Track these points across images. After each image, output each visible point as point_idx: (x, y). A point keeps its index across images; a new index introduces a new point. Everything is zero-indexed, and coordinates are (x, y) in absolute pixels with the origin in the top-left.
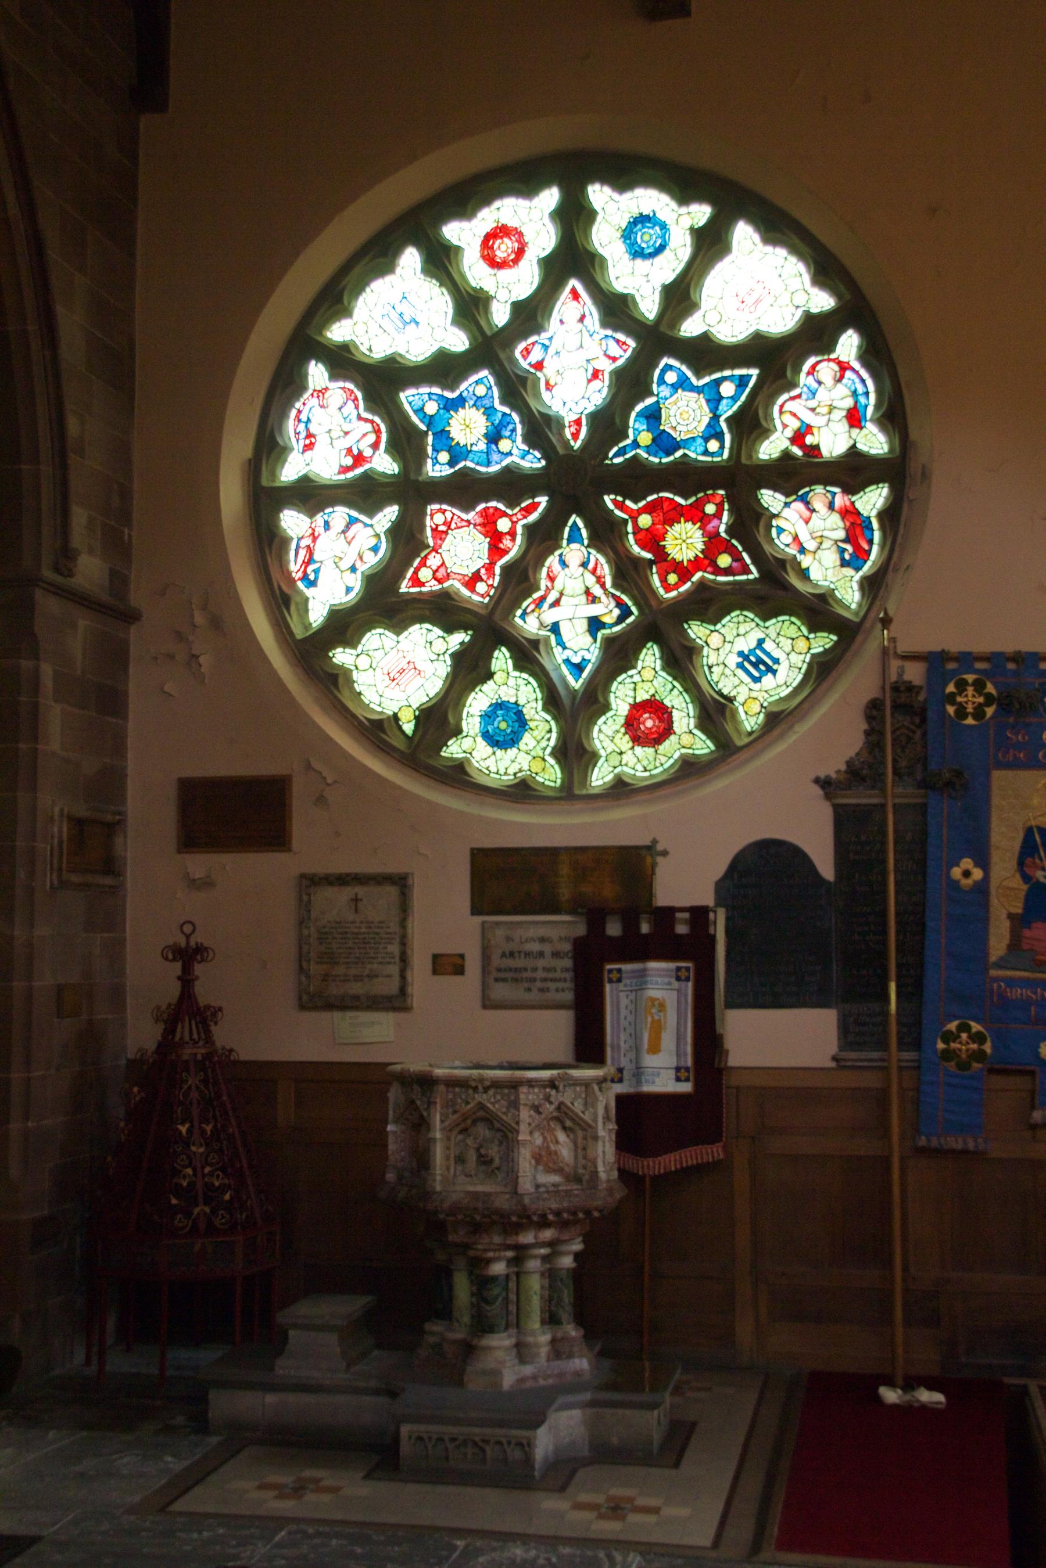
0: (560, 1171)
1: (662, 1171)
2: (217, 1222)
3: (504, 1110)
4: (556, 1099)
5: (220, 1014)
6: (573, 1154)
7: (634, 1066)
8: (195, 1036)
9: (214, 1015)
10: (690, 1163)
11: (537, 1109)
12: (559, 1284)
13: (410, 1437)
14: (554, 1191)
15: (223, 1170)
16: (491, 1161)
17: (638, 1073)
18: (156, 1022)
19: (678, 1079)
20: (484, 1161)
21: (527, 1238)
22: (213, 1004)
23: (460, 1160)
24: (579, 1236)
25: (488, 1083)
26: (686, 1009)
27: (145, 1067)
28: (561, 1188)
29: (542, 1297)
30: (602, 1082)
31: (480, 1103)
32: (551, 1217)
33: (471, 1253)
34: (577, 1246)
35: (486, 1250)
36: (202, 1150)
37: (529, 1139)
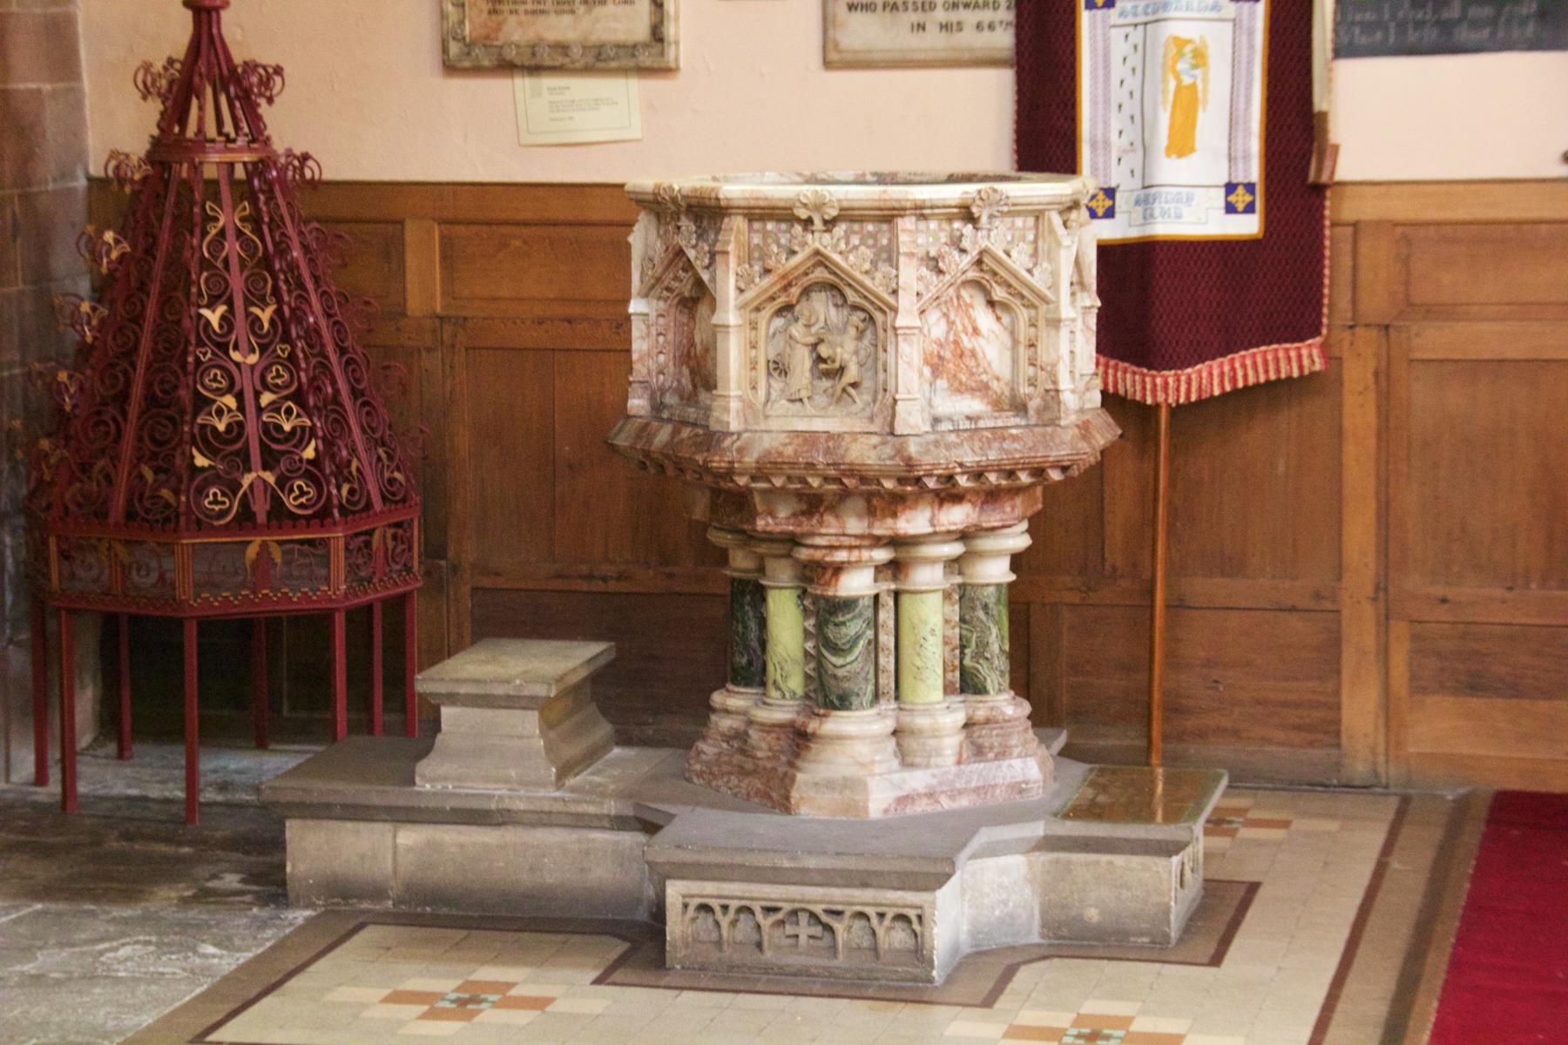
0: (983, 389)
1: (1194, 398)
2: (290, 502)
3: (867, 266)
4: (975, 243)
5: (278, 79)
6: (1007, 355)
7: (1137, 182)
8: (229, 128)
9: (266, 83)
10: (1251, 381)
11: (934, 264)
12: (981, 614)
13: (686, 906)
14: (972, 429)
15: (298, 397)
16: (842, 370)
17: (1147, 196)
18: (144, 98)
19: (1230, 209)
20: (827, 369)
21: (914, 522)
22: (264, 60)
23: (779, 368)
24: (1021, 520)
25: (834, 213)
26: (1250, 63)
27: (128, 189)
28: (982, 424)
29: (946, 641)
30: (1070, 209)
31: (817, 253)
32: (963, 481)
33: (804, 554)
34: (1018, 540)
35: (832, 548)
36: (253, 359)
37: (918, 327)
